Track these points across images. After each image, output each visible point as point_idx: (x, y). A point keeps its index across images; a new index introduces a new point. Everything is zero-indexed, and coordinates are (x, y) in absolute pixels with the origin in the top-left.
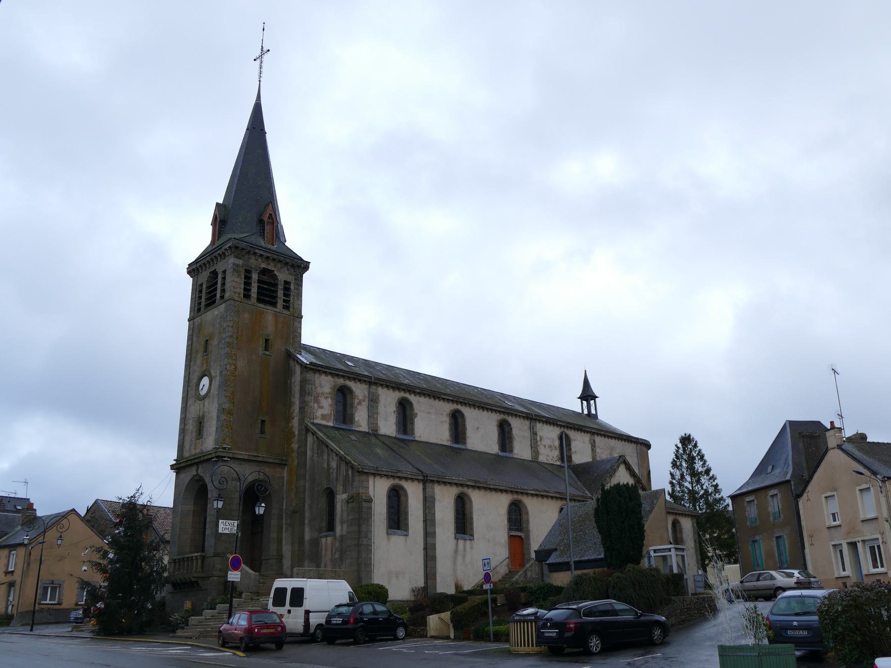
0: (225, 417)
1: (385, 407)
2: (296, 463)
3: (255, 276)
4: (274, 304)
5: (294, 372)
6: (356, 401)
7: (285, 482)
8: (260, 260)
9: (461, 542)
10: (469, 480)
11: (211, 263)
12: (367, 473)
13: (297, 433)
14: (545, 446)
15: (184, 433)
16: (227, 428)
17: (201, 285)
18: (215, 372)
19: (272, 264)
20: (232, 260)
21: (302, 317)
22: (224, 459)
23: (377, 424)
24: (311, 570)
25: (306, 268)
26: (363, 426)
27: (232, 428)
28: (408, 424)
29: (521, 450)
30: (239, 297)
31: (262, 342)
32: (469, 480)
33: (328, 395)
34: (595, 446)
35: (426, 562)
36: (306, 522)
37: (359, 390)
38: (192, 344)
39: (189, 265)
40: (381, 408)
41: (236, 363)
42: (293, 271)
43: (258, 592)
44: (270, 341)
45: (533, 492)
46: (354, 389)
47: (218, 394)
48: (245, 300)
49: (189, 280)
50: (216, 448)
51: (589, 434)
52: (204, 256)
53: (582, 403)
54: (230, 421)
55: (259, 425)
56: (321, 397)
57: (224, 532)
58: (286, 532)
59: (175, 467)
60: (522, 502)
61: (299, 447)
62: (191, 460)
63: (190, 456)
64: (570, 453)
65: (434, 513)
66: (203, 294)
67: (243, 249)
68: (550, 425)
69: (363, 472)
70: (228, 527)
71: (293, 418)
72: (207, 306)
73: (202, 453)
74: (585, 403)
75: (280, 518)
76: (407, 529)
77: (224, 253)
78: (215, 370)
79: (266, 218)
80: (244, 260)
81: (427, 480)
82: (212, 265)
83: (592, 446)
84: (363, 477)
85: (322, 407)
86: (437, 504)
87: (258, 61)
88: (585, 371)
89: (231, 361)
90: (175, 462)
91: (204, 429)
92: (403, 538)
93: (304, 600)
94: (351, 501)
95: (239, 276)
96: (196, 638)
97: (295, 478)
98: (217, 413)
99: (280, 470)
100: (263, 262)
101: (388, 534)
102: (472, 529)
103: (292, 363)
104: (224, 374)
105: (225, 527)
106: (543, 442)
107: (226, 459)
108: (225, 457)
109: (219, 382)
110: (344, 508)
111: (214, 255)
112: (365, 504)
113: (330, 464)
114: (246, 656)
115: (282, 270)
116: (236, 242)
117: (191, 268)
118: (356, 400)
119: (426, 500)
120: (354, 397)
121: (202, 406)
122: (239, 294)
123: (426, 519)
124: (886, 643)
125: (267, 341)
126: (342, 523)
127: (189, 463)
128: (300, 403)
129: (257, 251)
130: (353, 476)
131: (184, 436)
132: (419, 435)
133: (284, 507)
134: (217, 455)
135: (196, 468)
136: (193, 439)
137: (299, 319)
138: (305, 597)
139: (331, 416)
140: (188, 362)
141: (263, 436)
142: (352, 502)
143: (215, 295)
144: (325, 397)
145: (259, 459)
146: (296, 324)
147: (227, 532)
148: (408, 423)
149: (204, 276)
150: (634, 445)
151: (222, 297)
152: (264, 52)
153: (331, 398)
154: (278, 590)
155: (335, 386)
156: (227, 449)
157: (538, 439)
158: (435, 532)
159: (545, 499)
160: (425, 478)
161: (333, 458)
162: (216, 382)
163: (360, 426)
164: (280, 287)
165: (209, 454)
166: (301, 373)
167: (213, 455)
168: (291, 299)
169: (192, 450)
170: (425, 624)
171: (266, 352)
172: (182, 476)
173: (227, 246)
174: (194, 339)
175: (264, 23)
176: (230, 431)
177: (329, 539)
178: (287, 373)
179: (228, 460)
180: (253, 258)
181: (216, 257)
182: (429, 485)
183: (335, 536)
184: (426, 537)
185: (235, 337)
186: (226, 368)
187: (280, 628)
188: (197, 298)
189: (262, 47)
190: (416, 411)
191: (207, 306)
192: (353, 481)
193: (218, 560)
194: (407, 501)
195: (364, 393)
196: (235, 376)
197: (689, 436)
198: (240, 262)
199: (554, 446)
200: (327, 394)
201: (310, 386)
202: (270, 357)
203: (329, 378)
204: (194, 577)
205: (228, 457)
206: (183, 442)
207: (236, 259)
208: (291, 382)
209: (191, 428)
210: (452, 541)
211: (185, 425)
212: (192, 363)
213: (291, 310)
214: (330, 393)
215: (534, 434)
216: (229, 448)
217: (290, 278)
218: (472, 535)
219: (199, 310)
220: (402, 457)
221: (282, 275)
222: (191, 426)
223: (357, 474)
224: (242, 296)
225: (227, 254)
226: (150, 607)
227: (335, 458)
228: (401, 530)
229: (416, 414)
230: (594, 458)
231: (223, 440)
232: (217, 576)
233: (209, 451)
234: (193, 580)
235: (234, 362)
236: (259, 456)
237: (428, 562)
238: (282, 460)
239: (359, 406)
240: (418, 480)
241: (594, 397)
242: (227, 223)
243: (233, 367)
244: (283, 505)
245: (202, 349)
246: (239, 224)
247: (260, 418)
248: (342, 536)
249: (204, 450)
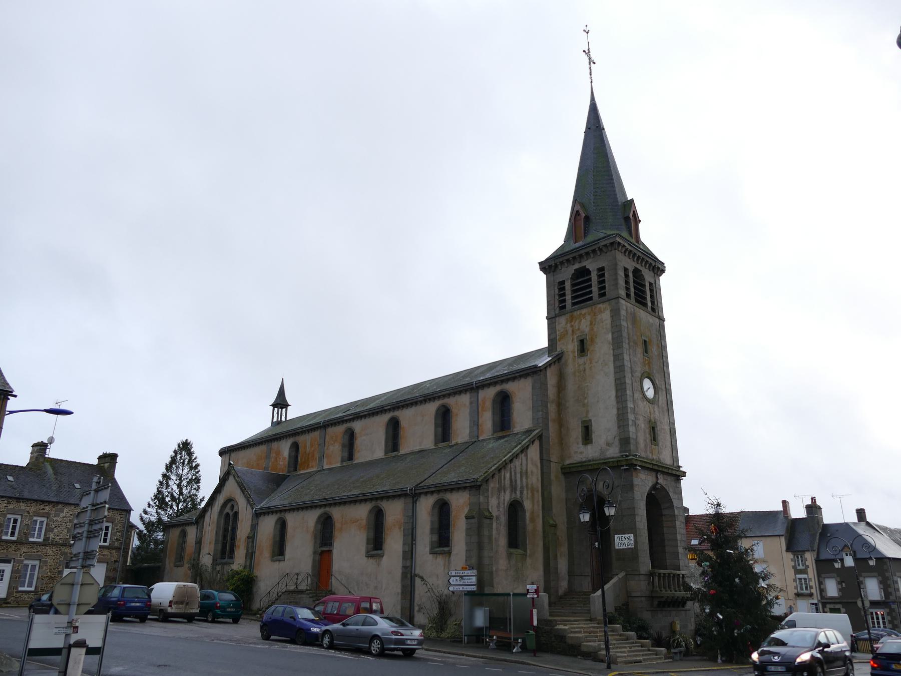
17: (563, 283)
49: (543, 277)
53: (274, 410)
57: (621, 548)
70: (624, 542)
105: (621, 542)
111: (648, 259)
125: (582, 342)
147: (624, 547)
149: (566, 273)
159: (358, 504)
165: (666, 468)
197: (187, 440)
220: (499, 470)
221: (648, 276)
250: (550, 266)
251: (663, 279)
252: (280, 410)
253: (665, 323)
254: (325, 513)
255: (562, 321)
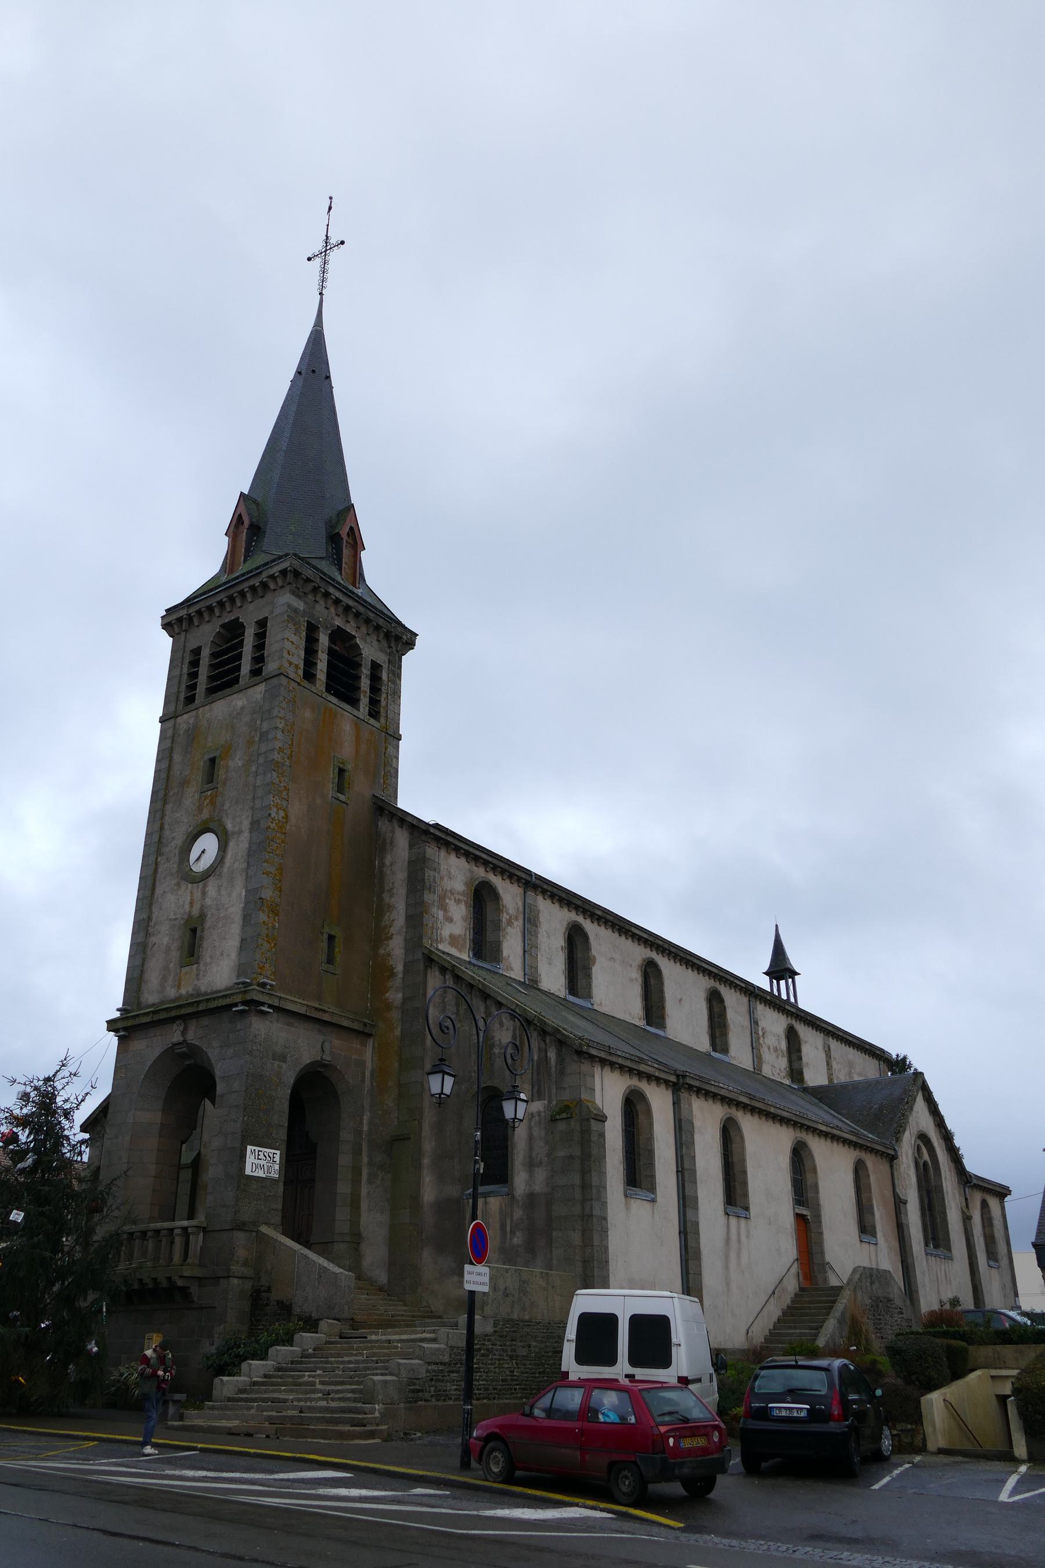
0: (265, 918)
1: (548, 937)
2: (398, 1032)
3: (324, 640)
4: (354, 702)
5: (392, 843)
6: (505, 917)
7: (368, 1074)
8: (332, 610)
9: (733, 1221)
10: (742, 1093)
11: (227, 605)
12: (592, 1058)
13: (399, 968)
14: (769, 1049)
15: (144, 953)
16: (268, 942)
17: (197, 652)
18: (239, 820)
19: (353, 623)
20: (285, 599)
21: (399, 738)
22: (263, 1008)
23: (536, 968)
24: (507, 1271)
25: (411, 644)
26: (515, 970)
27: (275, 944)
28: (580, 977)
29: (740, 1054)
30: (296, 673)
31: (333, 773)
32: (742, 1093)
33: (461, 897)
34: (830, 1057)
35: (687, 1261)
36: (426, 1161)
37: (510, 894)
38: (169, 768)
39: (167, 611)
40: (543, 939)
41: (287, 807)
42: (386, 645)
43: (352, 1319)
44: (347, 774)
45: (823, 1128)
46: (501, 891)
47: (248, 868)
48: (305, 683)
49: (165, 642)
50: (244, 983)
51: (822, 1034)
52: (201, 595)
54: (274, 927)
55: (324, 945)
56: (450, 899)
58: (370, 1182)
59: (119, 1025)
60: (807, 1147)
61: (405, 1000)
62: (167, 1010)
63: (163, 1002)
64: (801, 1065)
65: (695, 1157)
66: (201, 668)
67: (308, 580)
68: (774, 1010)
69: (588, 1053)
70: (262, 1162)
71: (391, 938)
72: (211, 691)
73: (198, 995)
74: (775, 981)
75: (357, 1152)
76: (652, 1189)
77: (264, 585)
78: (238, 820)
79: (344, 532)
80: (305, 603)
81: (683, 1084)
82: (228, 609)
83: (827, 1055)
84: (585, 1067)
85: (450, 920)
86: (697, 1137)
87: (318, 261)
88: (777, 926)
89: (278, 801)
90: (118, 1014)
91: (205, 945)
92: (648, 1205)
93: (674, 1349)
94: (564, 1115)
95: (297, 632)
96: (268, 1436)
97: (396, 1065)
98: (244, 909)
99: (358, 1046)
100: (339, 616)
101: (626, 1196)
102: (746, 1195)
103: (384, 825)
104: (263, 825)
106: (766, 1041)
107: (265, 1009)
108: (263, 1004)
109: (250, 843)
110: (535, 1134)
111: (239, 588)
112: (594, 1125)
113: (493, 1037)
114: (454, 1498)
115: (368, 639)
116: (296, 563)
117: (175, 616)
118: (505, 915)
119: (680, 1128)
120: (501, 907)
121: (198, 894)
122: (297, 666)
123: (683, 1169)
124: (504, 1387)
125: (341, 771)
126: (531, 1165)
127: (163, 1016)
128: (408, 905)
129: (331, 590)
130: (561, 1061)
131: (144, 960)
132: (599, 1002)
133: (365, 1128)
134: (248, 997)
135: (182, 1028)
136: (172, 965)
137: (395, 742)
138: (674, 1340)
139: (464, 940)
140: (159, 805)
141: (331, 968)
142: (568, 1118)
143: (238, 668)
144: (455, 900)
145: (326, 1017)
146: (390, 749)
147: (260, 1174)
148: (580, 975)
149: (205, 635)
150: (875, 1062)
151: (256, 672)
152: (328, 246)
153: (466, 904)
154: (587, 1320)
155: (472, 880)
156: (268, 987)
157: (761, 1033)
158: (697, 1198)
160: (681, 1080)
161: (501, 1024)
162: (239, 847)
163: (509, 968)
164: (365, 671)
166: (411, 846)
167: (238, 999)
168: (382, 699)
169: (168, 988)
170: (916, 1416)
171: (339, 795)
172: (139, 1045)
173: (275, 570)
174: (177, 757)
175: (331, 198)
176: (273, 950)
177: (494, 1204)
178: (378, 845)
179: (269, 1012)
180: (322, 602)
181: (253, 588)
182: (684, 1095)
183: (511, 1195)
184: (684, 1206)
185: (288, 752)
186: (270, 815)
187: (717, 1434)
188: (185, 677)
189: (327, 236)
190: (594, 952)
191: (211, 691)
192: (562, 1072)
193: (240, 1237)
194: (651, 1125)
195: (517, 904)
196: (285, 833)
197: (905, 1058)
198: (300, 605)
199: (780, 1048)
200: (458, 893)
201: (432, 873)
202: (344, 805)
203: (462, 862)
204: (181, 1277)
205: (270, 1006)
206: (142, 971)
207: (293, 597)
208: (382, 865)
209: (166, 940)
210: (721, 1218)
211: (148, 935)
212: (169, 807)
213: (382, 720)
214: (463, 894)
215: (754, 1022)
216: (271, 985)
217: (382, 658)
218: (747, 1209)
219: (190, 700)
221: (370, 650)
222: (165, 937)
223: (575, 1058)
224: (301, 672)
225: (272, 586)
226: (95, 1349)
227: (507, 1022)
228: (640, 1187)
229: (595, 957)
230: (830, 1080)
231: (260, 968)
232: (239, 1277)
233: (220, 991)
234: (180, 1283)
235: (285, 803)
236: (325, 1011)
237: (690, 1261)
238: (365, 1025)
239: (509, 927)
240: (667, 1082)
241: (793, 974)
242: (264, 533)
243: (282, 813)
244: (361, 1123)
245: (198, 778)
246: (290, 537)
247: (326, 930)
248: (531, 1196)
249: (203, 989)
250: (180, 620)
251: (409, 661)
252: (790, 980)
253: (402, 744)
254: (171, 1053)
255: (185, 721)
